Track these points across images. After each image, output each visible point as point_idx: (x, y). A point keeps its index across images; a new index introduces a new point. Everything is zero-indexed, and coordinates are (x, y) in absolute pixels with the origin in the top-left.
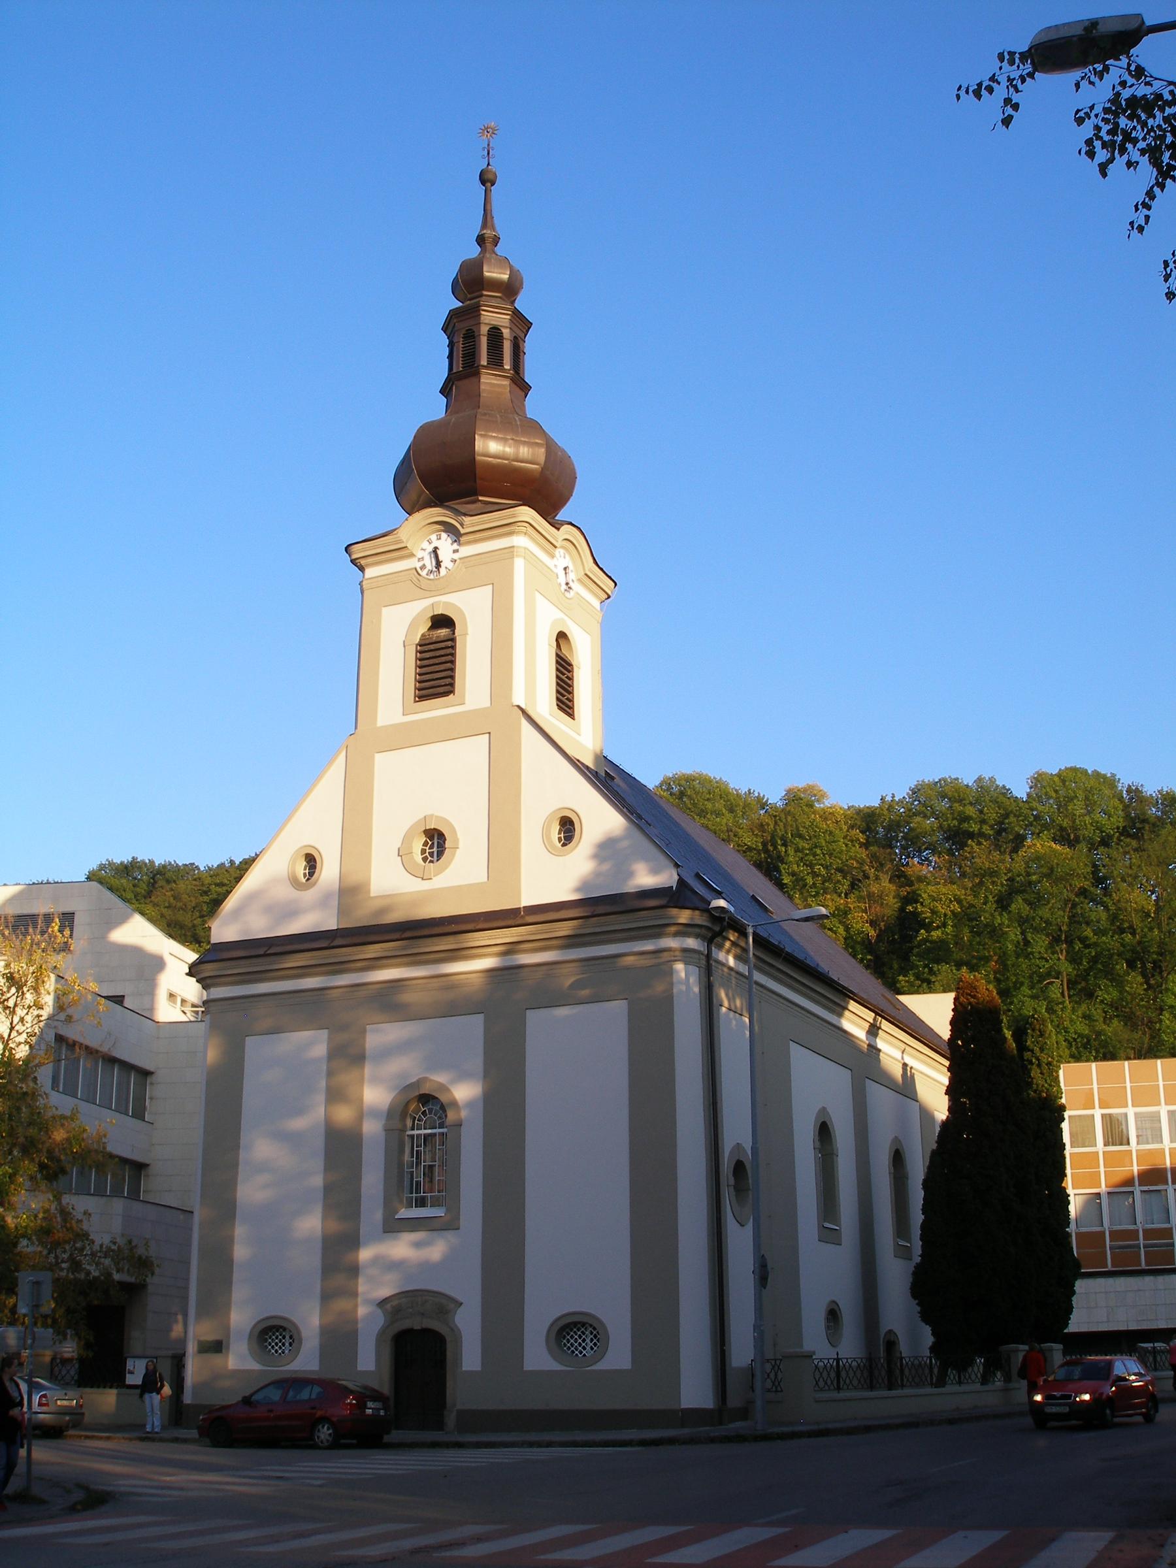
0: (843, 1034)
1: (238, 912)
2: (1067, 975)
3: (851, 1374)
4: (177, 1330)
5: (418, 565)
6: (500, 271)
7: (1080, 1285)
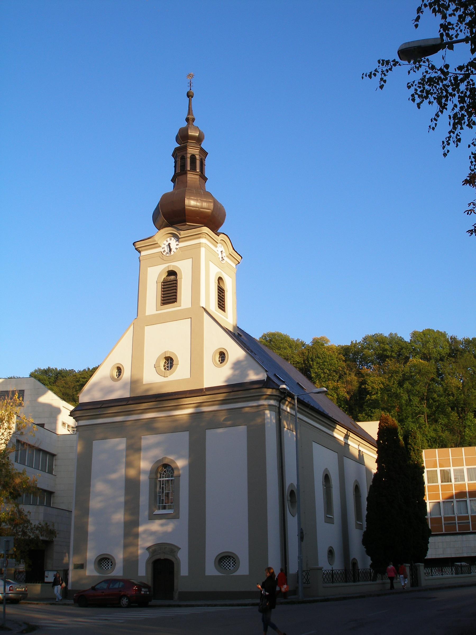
0: (334, 438)
1: (89, 391)
2: (427, 413)
3: (338, 576)
4: (66, 560)
5: (162, 250)
6: (195, 132)
7: (431, 539)
